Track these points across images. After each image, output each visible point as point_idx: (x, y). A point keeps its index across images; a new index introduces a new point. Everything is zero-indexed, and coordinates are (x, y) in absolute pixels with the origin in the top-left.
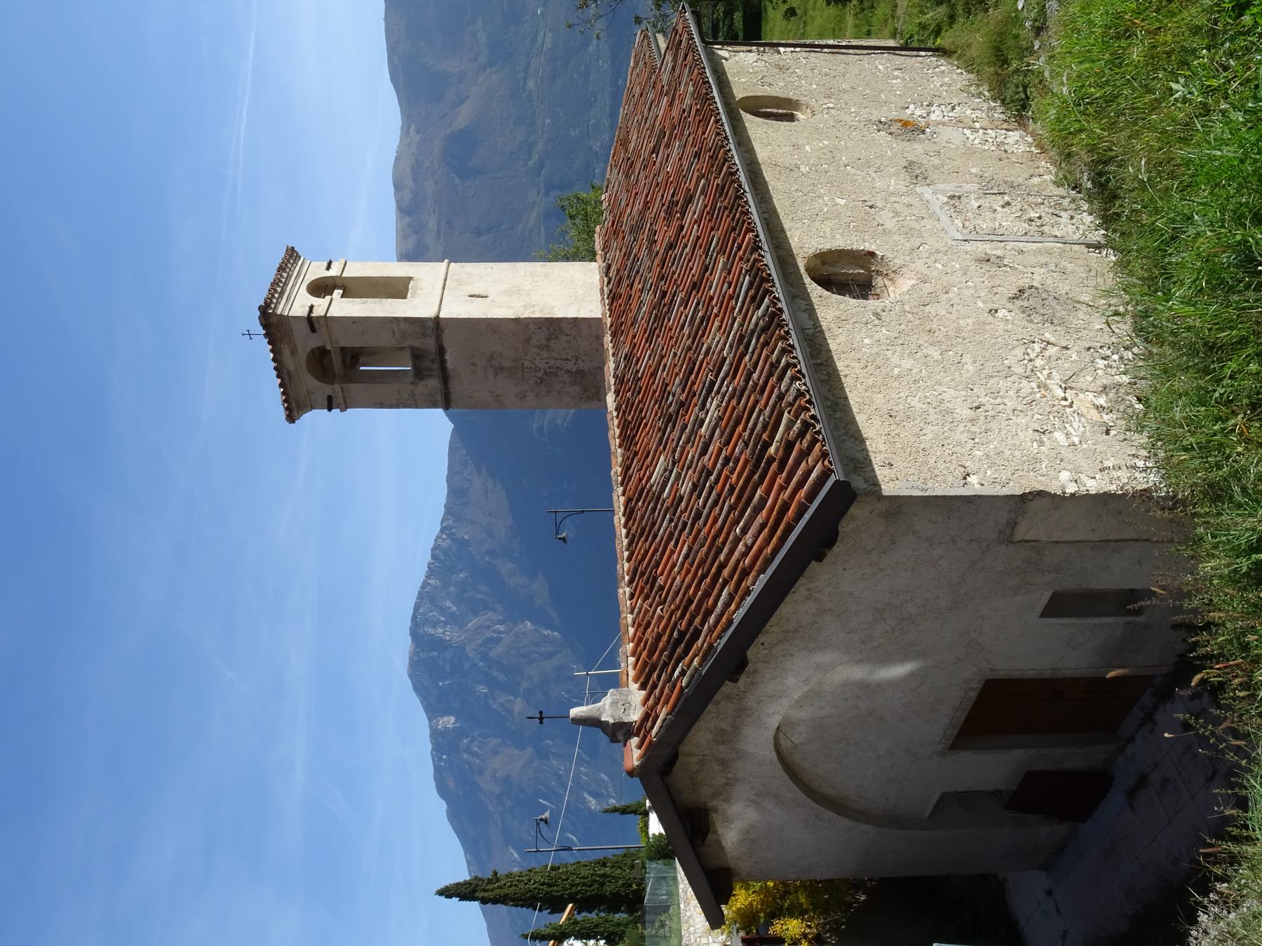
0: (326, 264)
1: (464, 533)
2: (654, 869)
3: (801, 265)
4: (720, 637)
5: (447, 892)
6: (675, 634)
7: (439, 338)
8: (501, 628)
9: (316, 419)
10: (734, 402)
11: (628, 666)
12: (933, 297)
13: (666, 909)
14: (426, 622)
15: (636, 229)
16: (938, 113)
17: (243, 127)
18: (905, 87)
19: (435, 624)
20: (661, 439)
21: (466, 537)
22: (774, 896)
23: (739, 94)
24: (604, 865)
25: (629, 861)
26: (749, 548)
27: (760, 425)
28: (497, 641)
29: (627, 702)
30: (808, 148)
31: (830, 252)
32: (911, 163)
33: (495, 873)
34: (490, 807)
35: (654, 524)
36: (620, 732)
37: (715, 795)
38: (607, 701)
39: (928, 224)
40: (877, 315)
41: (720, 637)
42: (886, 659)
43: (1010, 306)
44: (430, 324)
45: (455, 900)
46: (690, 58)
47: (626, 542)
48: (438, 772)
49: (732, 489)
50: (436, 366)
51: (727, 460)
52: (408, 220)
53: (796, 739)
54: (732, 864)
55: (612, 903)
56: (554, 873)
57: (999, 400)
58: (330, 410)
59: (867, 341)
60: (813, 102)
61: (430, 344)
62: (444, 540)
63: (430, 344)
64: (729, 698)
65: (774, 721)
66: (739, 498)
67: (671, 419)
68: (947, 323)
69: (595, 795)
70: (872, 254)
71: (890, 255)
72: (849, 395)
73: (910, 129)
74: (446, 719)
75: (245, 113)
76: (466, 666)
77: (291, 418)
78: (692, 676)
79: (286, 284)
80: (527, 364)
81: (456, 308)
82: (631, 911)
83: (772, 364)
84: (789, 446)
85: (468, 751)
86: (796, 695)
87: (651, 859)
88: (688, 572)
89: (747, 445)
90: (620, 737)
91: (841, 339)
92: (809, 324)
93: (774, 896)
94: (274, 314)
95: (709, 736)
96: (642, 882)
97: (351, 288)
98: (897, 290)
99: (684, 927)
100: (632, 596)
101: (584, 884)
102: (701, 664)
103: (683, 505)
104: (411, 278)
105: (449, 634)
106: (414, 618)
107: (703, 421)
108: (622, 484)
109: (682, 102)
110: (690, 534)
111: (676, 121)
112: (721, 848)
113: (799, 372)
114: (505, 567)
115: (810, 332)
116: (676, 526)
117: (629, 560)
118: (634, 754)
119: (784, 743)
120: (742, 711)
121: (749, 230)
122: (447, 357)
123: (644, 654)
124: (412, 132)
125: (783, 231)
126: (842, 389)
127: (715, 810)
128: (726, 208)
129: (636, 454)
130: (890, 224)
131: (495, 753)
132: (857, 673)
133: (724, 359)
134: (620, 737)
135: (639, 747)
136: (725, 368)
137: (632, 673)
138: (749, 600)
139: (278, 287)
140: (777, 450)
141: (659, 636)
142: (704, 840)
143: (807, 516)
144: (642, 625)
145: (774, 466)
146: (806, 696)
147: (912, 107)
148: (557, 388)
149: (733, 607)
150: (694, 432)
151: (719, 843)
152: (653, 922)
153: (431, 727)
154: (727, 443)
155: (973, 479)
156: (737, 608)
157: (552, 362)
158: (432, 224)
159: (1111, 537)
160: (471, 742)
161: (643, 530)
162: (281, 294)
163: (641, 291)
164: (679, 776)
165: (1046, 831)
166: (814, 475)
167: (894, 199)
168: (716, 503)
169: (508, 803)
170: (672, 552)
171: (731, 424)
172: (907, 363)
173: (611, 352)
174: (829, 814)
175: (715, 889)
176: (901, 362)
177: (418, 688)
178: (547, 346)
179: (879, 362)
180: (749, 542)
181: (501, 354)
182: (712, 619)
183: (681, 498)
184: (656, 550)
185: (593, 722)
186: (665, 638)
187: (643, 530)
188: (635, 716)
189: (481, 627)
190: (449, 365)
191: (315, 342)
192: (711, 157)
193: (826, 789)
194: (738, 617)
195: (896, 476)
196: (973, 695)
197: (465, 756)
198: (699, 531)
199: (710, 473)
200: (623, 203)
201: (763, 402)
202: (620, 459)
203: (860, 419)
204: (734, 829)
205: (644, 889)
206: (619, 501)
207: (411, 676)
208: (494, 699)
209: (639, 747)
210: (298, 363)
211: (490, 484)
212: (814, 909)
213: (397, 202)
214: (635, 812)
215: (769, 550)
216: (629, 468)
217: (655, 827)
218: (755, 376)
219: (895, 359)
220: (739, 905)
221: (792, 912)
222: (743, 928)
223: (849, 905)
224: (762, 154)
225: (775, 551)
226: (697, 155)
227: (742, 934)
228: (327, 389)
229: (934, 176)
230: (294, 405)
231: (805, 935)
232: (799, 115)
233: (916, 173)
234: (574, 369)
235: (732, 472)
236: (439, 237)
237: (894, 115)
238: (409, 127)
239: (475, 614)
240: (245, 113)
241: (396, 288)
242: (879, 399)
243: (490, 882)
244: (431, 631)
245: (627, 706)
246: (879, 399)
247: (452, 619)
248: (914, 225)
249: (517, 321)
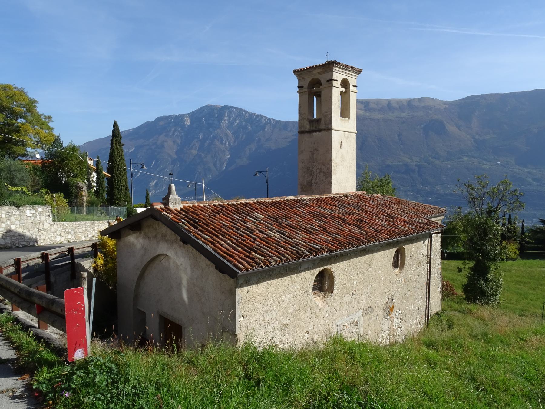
0: (356, 85)
1: (268, 129)
2: (123, 210)
3: (328, 267)
4: (194, 235)
5: (115, 125)
6: (197, 221)
7: (325, 130)
8: (227, 144)
9: (295, 81)
10: (275, 242)
11: (189, 204)
12: (313, 312)
13: (108, 214)
14: (230, 112)
15: (358, 208)
16: (397, 322)
17: (448, 30)
18: (410, 310)
19: (229, 116)
20: (270, 216)
21: (266, 130)
22: (111, 255)
23: (406, 247)
24: (126, 189)
25: (127, 199)
26: (222, 245)
27: (263, 250)
28: (222, 143)
29: (176, 203)
30: (380, 272)
31: (333, 277)
32: (373, 309)
33: (123, 145)
34: (152, 140)
35: (239, 213)
36: (166, 201)
37: (145, 234)
38: (177, 197)
39: (345, 313)
40: (306, 292)
41: (194, 235)
42: (189, 291)
43: (310, 338)
44: (329, 127)
45: (112, 129)
46: (420, 229)
47: (235, 203)
48: (166, 118)
49: (244, 241)
50: (314, 128)
51: (255, 239)
52: (405, 104)
53: (163, 261)
54: (122, 239)
55: (111, 193)
56: (122, 169)
57: (272, 330)
58: (298, 87)
59: (296, 288)
60: (402, 275)
61: (322, 126)
62: (265, 120)
63: (322, 126)
64: (176, 239)
65: (169, 254)
66: (240, 243)
67: (277, 220)
68: (303, 316)
69: (156, 184)
70: (332, 292)
71: (332, 298)
72: (274, 280)
73: (390, 310)
74: (189, 121)
75: (454, 31)
76: (211, 130)
77: (295, 72)
78: (182, 226)
79: (346, 70)
80: (315, 164)
81: (336, 137)
82: (107, 200)
83: (283, 254)
84: (253, 259)
85: (175, 131)
86: (177, 261)
87: (127, 209)
88: (219, 225)
89: (258, 246)
90: (164, 201)
91: (297, 279)
92: (302, 268)
93: (111, 255)
94: (334, 66)
95: (164, 231)
96: (119, 205)
97: (345, 96)
98: (318, 300)
99: (101, 222)
100: (214, 205)
101: (118, 182)
102: (186, 229)
103: (243, 224)
104: (349, 118)
105: (225, 122)
106: (231, 107)
107: (272, 231)
108: (257, 202)
109: (403, 226)
110: (232, 226)
111: (396, 223)
112: (128, 235)
113: (279, 263)
114: (253, 147)
115: (299, 268)
116: (236, 221)
117: (228, 204)
118: (158, 206)
119: (163, 257)
120: (172, 243)
121: (337, 248)
122: (317, 133)
123: (192, 210)
124: (445, 106)
125: (342, 261)
126: (277, 278)
127: (140, 233)
128: (350, 241)
129: (267, 207)
130: (345, 299)
131: (174, 142)
132: (185, 282)
133: (292, 239)
134: (164, 201)
135: (160, 208)
136: (288, 239)
137: (187, 205)
138: (204, 245)
139: (345, 67)
140: (253, 255)
141: (197, 215)
142: (130, 229)
143: (228, 263)
144: (203, 209)
145: (248, 254)
146: (177, 265)
147: (400, 312)
149: (203, 240)
150: (269, 228)
151: (129, 235)
152: (103, 209)
153: (185, 114)
154: (261, 239)
155: (242, 318)
156: (202, 241)
157: (315, 173)
158: (404, 115)
160: (179, 132)
161: (238, 210)
162: (342, 69)
163: (331, 210)
164: (151, 221)
166: (241, 266)
167: (356, 302)
168: (241, 235)
169: (153, 148)
170: (227, 220)
171: (267, 241)
172: (287, 301)
173: (311, 198)
174: (139, 273)
175: (114, 233)
176: (287, 300)
177: (201, 109)
178: (321, 172)
179: (287, 291)
180: (224, 246)
182: (200, 233)
183: (246, 223)
184: (229, 214)
185: (170, 192)
186: (197, 217)
187: (238, 210)
188: (171, 207)
189: (228, 136)
190: (314, 134)
191: (323, 82)
192: (373, 236)
194: (199, 241)
195: (243, 294)
196: (177, 322)
197: (173, 129)
198: (232, 229)
199: (252, 233)
200: (371, 202)
201: (272, 251)
202: (267, 201)
203: (265, 283)
204: (134, 240)
205: (116, 206)
206: (251, 201)
207: (207, 106)
208: (197, 142)
209: (160, 208)
210: (315, 74)
211: (289, 140)
212: (107, 270)
213: (414, 99)
214: (147, 202)
215: (220, 252)
216: (263, 204)
217: (140, 210)
218: (282, 249)
219: (288, 297)
220: (108, 242)
221: (105, 261)
222: (100, 243)
223: (108, 282)
224: (377, 255)
225: (219, 254)
226: (377, 231)
227: (98, 243)
228: (306, 86)
229: (367, 317)
230: (300, 73)
231: (97, 265)
232: (397, 270)
233: (368, 311)
235: (250, 241)
236: (397, 118)
237: (396, 305)
238: (447, 104)
239: (233, 134)
240: (454, 31)
241: (345, 113)
242: (272, 290)
243: (119, 143)
244: (226, 114)
245: (175, 204)
246: (272, 290)
247: (231, 124)
248: (345, 308)
249: (330, 160)
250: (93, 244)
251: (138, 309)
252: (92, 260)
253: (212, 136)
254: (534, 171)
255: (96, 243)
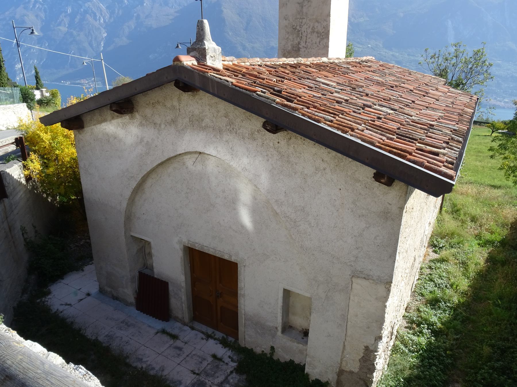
8: (102, 21)
21: (145, 4)
34: (7, 13)
36: (200, 53)
37: (145, 117)
42: (255, 211)
65: (210, 150)
80: (304, 21)
114: (132, 24)
131: (37, 16)
148: (291, 37)
151: (105, 120)
157: (305, 34)
159: (349, 323)
165: (129, 292)
174: (134, 184)
178: (314, 32)
181: (310, 6)
189: (101, 11)
193: (149, 182)
196: (226, 257)
204: (114, 129)
208: (65, 16)
221: (45, 166)
234: (300, 46)
239: (107, 8)
249: (329, 15)
250: (16, 139)
251: (132, 236)
252: (20, 164)
253: (82, 10)
254: (397, 54)
255: (21, 138)
